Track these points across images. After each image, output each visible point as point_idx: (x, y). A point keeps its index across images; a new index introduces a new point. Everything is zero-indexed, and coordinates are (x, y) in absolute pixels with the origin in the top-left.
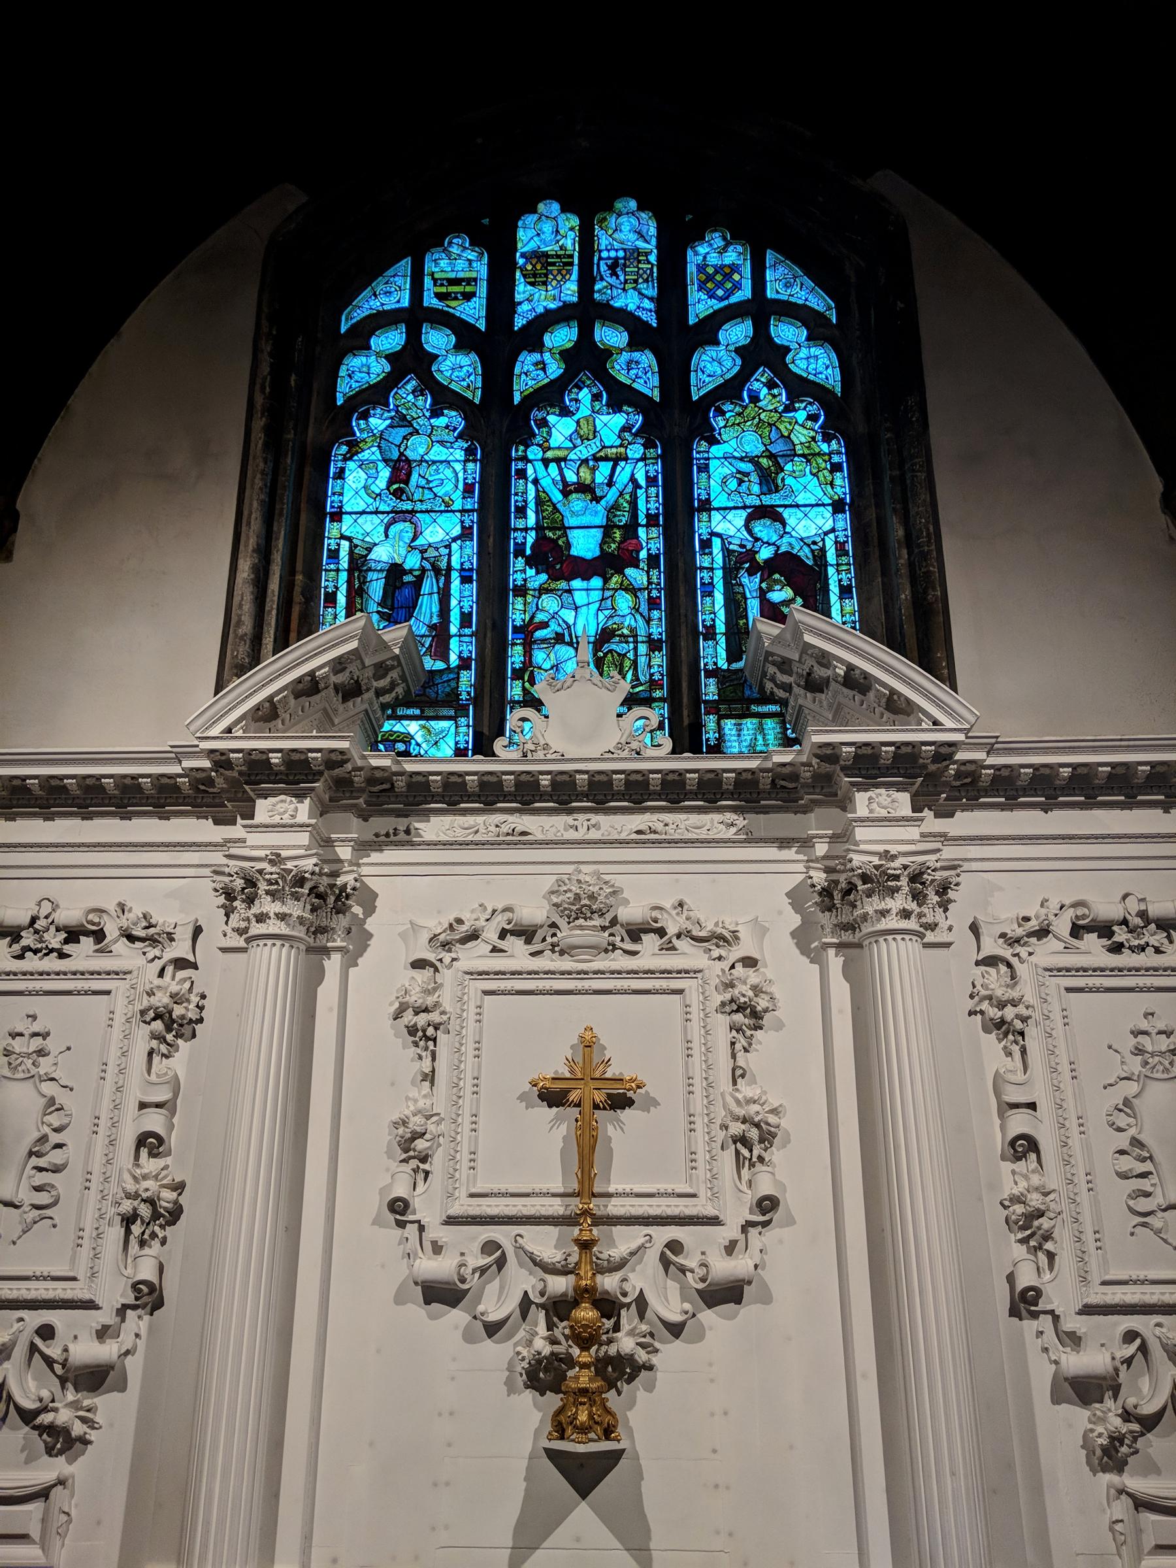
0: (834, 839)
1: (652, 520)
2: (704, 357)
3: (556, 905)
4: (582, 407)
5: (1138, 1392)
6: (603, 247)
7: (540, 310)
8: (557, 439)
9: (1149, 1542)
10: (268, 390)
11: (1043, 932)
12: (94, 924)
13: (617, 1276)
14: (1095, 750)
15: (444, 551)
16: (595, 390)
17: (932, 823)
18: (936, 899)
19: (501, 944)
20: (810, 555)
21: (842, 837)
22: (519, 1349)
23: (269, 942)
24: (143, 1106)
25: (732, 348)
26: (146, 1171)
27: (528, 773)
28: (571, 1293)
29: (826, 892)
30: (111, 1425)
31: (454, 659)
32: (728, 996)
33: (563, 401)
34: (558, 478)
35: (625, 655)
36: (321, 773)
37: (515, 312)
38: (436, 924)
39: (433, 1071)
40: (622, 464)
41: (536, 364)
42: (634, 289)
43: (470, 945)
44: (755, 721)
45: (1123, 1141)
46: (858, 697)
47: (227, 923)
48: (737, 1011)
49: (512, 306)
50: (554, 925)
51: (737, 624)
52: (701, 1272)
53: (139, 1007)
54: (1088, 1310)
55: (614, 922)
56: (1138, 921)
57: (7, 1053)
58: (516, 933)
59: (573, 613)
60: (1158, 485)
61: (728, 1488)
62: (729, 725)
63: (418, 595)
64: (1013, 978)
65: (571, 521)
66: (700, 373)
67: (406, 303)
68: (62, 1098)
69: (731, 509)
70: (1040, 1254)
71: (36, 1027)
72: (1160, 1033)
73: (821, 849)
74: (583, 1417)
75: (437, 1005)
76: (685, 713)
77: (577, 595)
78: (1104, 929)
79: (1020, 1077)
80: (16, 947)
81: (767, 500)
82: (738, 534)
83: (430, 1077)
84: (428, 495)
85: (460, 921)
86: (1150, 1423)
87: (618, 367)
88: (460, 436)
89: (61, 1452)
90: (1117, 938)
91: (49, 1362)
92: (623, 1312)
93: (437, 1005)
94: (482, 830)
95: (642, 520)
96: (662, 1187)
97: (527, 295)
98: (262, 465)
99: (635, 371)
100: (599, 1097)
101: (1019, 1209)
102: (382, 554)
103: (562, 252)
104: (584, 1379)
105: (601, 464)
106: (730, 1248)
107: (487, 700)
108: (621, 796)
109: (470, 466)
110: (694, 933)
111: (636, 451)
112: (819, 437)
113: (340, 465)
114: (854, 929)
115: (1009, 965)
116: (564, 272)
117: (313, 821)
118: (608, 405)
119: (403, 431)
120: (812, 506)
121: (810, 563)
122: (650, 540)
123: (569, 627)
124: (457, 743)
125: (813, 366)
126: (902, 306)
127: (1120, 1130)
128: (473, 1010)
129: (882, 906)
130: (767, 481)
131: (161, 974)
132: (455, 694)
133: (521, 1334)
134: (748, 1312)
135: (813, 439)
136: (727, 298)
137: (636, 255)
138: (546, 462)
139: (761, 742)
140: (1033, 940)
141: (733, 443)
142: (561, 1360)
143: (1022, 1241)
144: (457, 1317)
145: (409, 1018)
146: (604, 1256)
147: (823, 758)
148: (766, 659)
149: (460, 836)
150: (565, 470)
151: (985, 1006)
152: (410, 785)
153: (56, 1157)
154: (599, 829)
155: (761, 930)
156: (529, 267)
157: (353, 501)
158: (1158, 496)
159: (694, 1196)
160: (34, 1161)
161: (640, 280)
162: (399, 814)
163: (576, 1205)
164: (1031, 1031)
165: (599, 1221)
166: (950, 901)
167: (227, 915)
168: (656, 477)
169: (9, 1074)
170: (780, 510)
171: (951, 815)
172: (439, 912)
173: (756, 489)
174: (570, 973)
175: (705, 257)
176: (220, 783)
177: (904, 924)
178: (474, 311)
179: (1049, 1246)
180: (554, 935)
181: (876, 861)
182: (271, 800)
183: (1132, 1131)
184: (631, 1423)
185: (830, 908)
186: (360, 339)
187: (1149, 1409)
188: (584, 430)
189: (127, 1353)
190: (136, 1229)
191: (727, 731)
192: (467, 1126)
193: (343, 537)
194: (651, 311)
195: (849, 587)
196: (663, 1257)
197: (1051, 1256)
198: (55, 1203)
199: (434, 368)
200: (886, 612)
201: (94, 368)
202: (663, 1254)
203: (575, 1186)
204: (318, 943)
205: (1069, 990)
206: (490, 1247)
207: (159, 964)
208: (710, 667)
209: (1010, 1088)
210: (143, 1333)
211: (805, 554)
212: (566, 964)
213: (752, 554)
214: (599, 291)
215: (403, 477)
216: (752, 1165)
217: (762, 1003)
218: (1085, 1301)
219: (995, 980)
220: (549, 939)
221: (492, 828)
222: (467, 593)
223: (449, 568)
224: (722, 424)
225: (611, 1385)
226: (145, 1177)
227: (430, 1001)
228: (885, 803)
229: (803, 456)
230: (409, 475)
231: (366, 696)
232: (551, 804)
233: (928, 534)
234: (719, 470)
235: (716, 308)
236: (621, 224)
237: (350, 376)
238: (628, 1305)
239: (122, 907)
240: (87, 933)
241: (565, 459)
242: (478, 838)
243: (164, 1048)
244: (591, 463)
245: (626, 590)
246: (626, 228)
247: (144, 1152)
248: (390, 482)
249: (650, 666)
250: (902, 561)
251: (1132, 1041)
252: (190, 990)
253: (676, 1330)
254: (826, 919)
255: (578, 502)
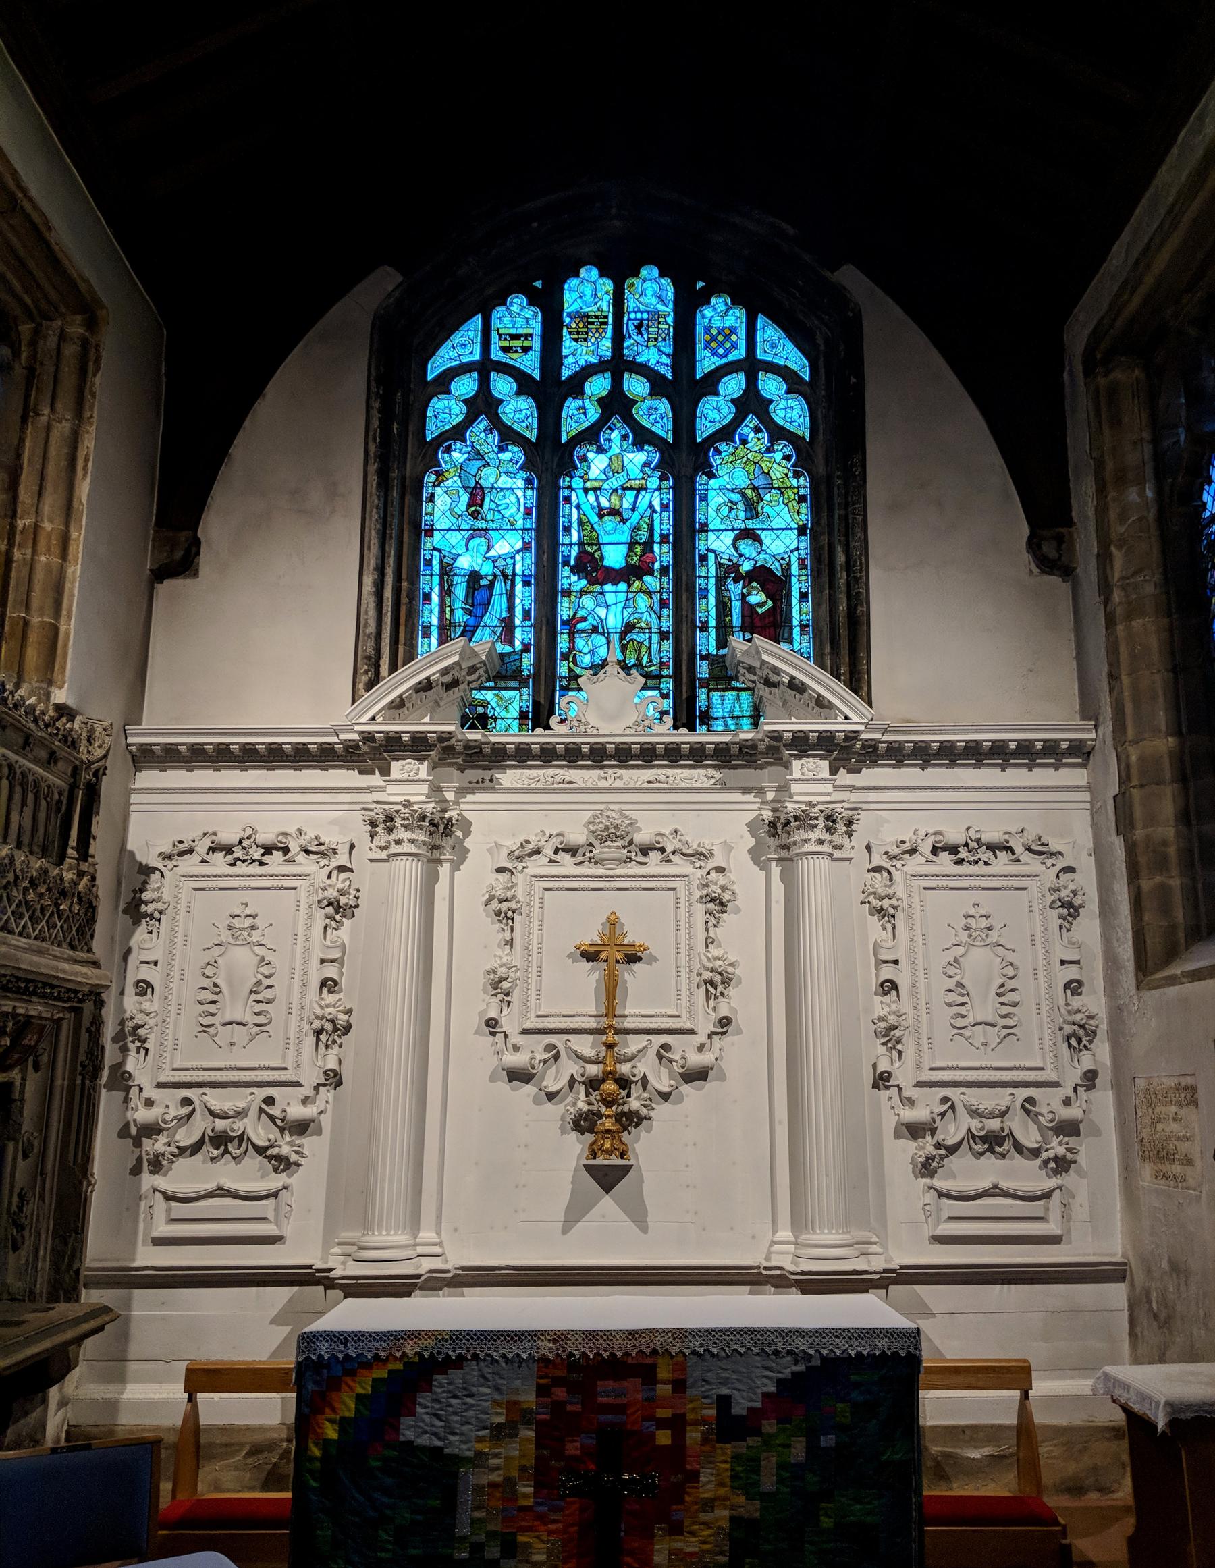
0: (779, 789)
1: (664, 539)
2: (707, 406)
3: (593, 832)
4: (613, 446)
5: (947, 1132)
6: (631, 309)
7: (582, 363)
8: (595, 472)
9: (945, 1215)
10: (378, 440)
11: (912, 851)
12: (282, 843)
13: (629, 1065)
14: (955, 732)
15: (510, 561)
16: (623, 432)
17: (844, 777)
18: (845, 829)
19: (555, 857)
20: (779, 568)
21: (783, 788)
22: (568, 1108)
23: (405, 858)
24: (323, 961)
25: (728, 398)
26: (328, 1002)
27: (574, 743)
28: (601, 1075)
29: (772, 825)
30: (314, 1155)
31: (518, 645)
32: (704, 892)
33: (599, 441)
34: (595, 504)
35: (642, 643)
36: (435, 745)
37: (562, 364)
38: (512, 844)
39: (512, 939)
40: (643, 493)
41: (578, 409)
42: (655, 346)
43: (534, 857)
44: (734, 693)
45: (951, 984)
46: (798, 695)
47: (371, 841)
48: (711, 902)
49: (560, 358)
50: (591, 845)
51: (725, 620)
52: (682, 1062)
53: (316, 899)
54: (920, 1085)
55: (631, 843)
56: (973, 845)
57: (230, 928)
58: (564, 850)
59: (605, 610)
60: (1026, 531)
61: (695, 1187)
62: (715, 696)
63: (491, 595)
64: (891, 880)
65: (604, 539)
66: (703, 419)
67: (477, 356)
68: (269, 956)
69: (722, 530)
70: (894, 1052)
71: (248, 911)
72: (982, 916)
73: (770, 795)
74: (608, 1145)
75: (514, 897)
76: (684, 689)
77: (607, 595)
78: (953, 850)
79: (890, 943)
80: (230, 858)
81: (750, 524)
82: (728, 551)
83: (510, 943)
84: (497, 516)
85: (528, 842)
86: (952, 1150)
87: (641, 413)
88: (521, 468)
89: (283, 1171)
90: (960, 856)
91: (272, 1118)
92: (633, 1086)
93: (514, 897)
94: (542, 779)
95: (657, 538)
96: (659, 1011)
97: (571, 350)
98: (376, 502)
99: (654, 417)
100: (620, 956)
101: (883, 1025)
102: (465, 563)
103: (599, 313)
104: (608, 1124)
105: (628, 492)
106: (701, 1048)
107: (543, 677)
108: (637, 758)
109: (529, 493)
110: (684, 851)
111: (653, 482)
112: (791, 474)
113: (430, 490)
114: (789, 848)
115: (889, 872)
116: (601, 331)
117: (431, 778)
118: (633, 444)
119: (479, 464)
120: (783, 529)
121: (779, 574)
122: (663, 554)
123: (602, 621)
124: (521, 707)
125: (789, 415)
126: (855, 380)
127: (950, 977)
128: (537, 900)
129: (805, 837)
130: (751, 510)
131: (329, 876)
132: (519, 670)
133: (570, 1099)
134: (710, 1086)
135: (787, 475)
136: (726, 356)
137: (657, 316)
138: (586, 491)
139: (738, 708)
140: (907, 856)
141: (726, 477)
142: (594, 1114)
143: (884, 1044)
144: (529, 1089)
145: (495, 905)
146: (622, 1052)
147: (772, 738)
148: (738, 664)
149: (526, 783)
150: (600, 498)
151: (871, 898)
152: (493, 749)
153: (267, 994)
154: (622, 779)
155: (728, 848)
156: (574, 325)
157: (441, 522)
158: (1025, 539)
159: (679, 1016)
160: (254, 997)
161: (660, 339)
162: (485, 768)
163: (604, 1022)
164: (900, 915)
165: (619, 1032)
166: (852, 831)
167: (372, 837)
168: (668, 504)
169: (233, 942)
170: (759, 532)
171: (859, 771)
172: (513, 835)
173: (742, 515)
174: (601, 877)
175: (710, 320)
176: (365, 748)
177: (820, 848)
178: (530, 363)
179: (899, 1047)
180: (591, 851)
181: (803, 807)
182: (401, 762)
183: (958, 978)
184: (637, 1151)
185: (774, 835)
186: (443, 384)
187: (951, 1141)
188: (615, 466)
189: (321, 1112)
190: (323, 1038)
191: (714, 701)
192: (534, 974)
193: (434, 549)
194: (667, 365)
195: (807, 593)
196: (659, 1054)
197: (900, 1053)
198: (270, 1023)
199: (500, 411)
200: (831, 616)
201: (247, 423)
202: (658, 1052)
203: (604, 1011)
204: (434, 857)
205: (925, 889)
206: (550, 1047)
207: (327, 869)
208: (704, 653)
209: (883, 951)
210: (331, 1100)
211: (776, 568)
212: (599, 871)
213: (737, 566)
214: (628, 347)
215: (478, 501)
216: (716, 997)
217: (726, 897)
218: (919, 1079)
219: (879, 879)
220: (588, 854)
221: (549, 779)
222: (527, 594)
223: (514, 574)
224: (719, 461)
225: (625, 1128)
226: (328, 1006)
227: (509, 894)
228: (812, 768)
229: (779, 489)
230: (483, 499)
231: (462, 687)
232: (589, 763)
233: (861, 563)
234: (715, 499)
235: (717, 364)
236: (645, 289)
237: (435, 416)
238: (636, 1082)
239: (300, 831)
240: (278, 849)
241: (600, 489)
242: (539, 785)
243: (334, 924)
244: (620, 492)
245: (644, 592)
246: (649, 293)
247: (325, 990)
248: (469, 505)
249: (660, 651)
250: (842, 581)
251: (964, 921)
252: (350, 886)
253: (665, 1096)
254: (772, 842)
255: (610, 523)
